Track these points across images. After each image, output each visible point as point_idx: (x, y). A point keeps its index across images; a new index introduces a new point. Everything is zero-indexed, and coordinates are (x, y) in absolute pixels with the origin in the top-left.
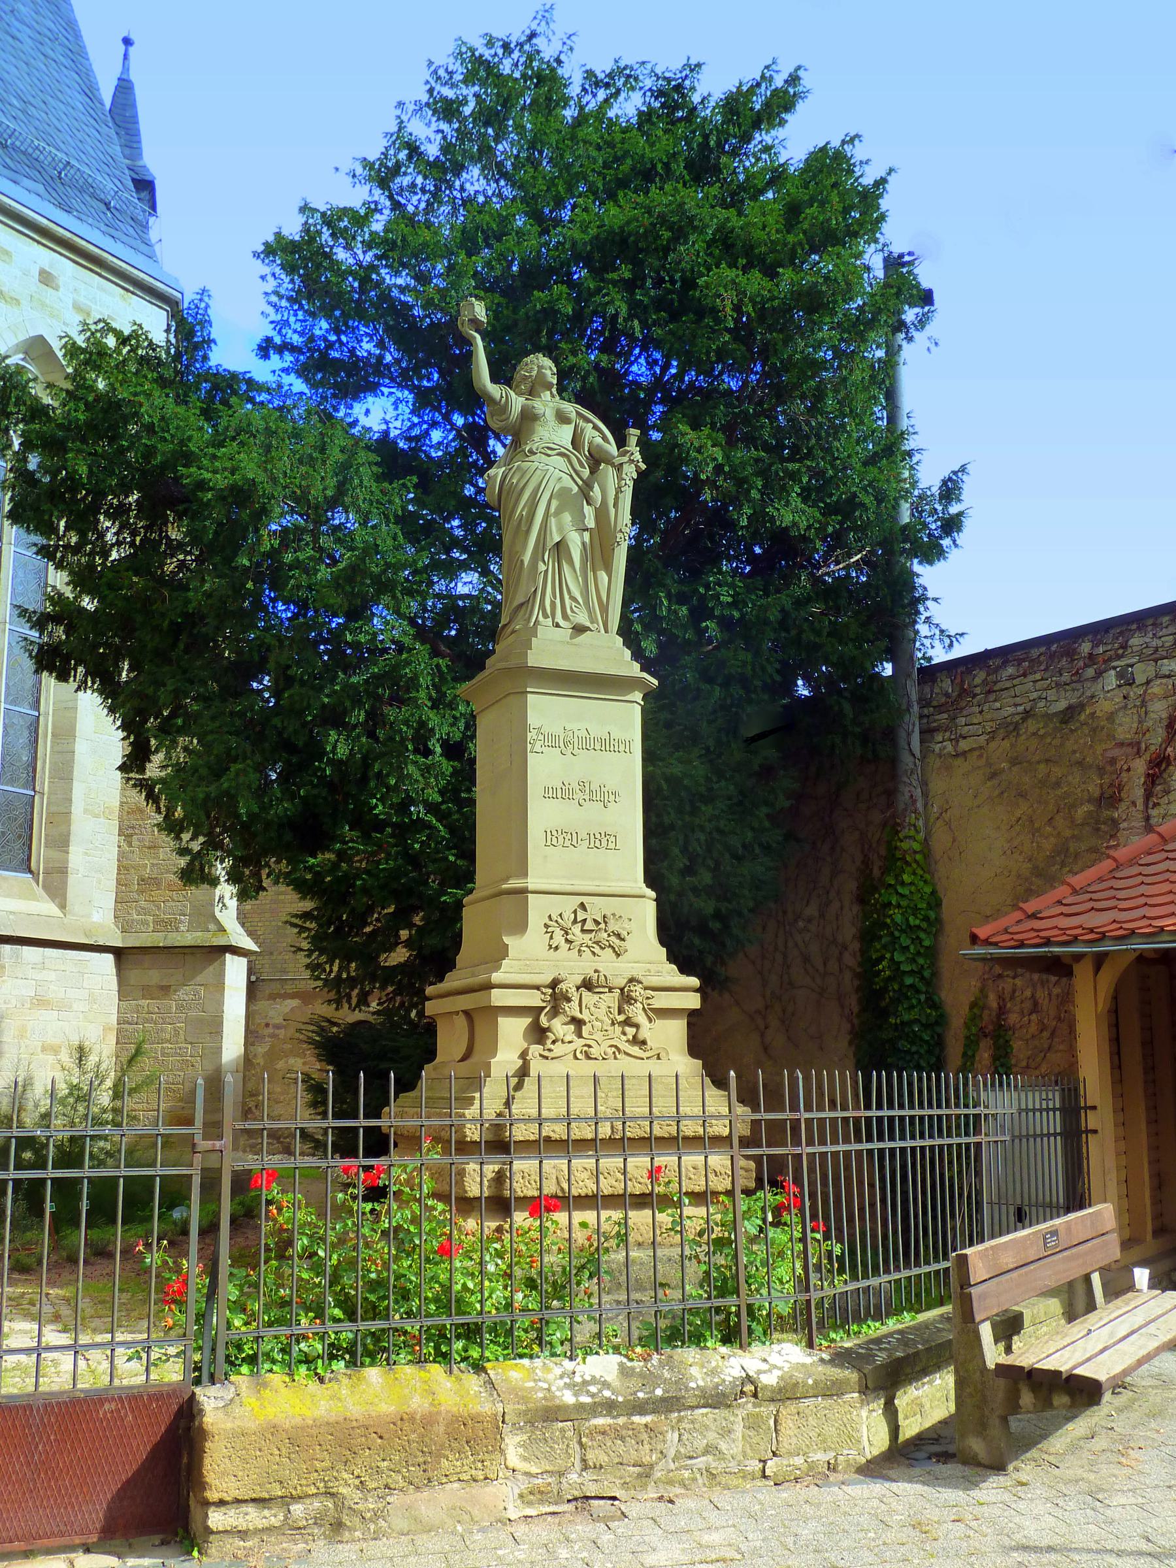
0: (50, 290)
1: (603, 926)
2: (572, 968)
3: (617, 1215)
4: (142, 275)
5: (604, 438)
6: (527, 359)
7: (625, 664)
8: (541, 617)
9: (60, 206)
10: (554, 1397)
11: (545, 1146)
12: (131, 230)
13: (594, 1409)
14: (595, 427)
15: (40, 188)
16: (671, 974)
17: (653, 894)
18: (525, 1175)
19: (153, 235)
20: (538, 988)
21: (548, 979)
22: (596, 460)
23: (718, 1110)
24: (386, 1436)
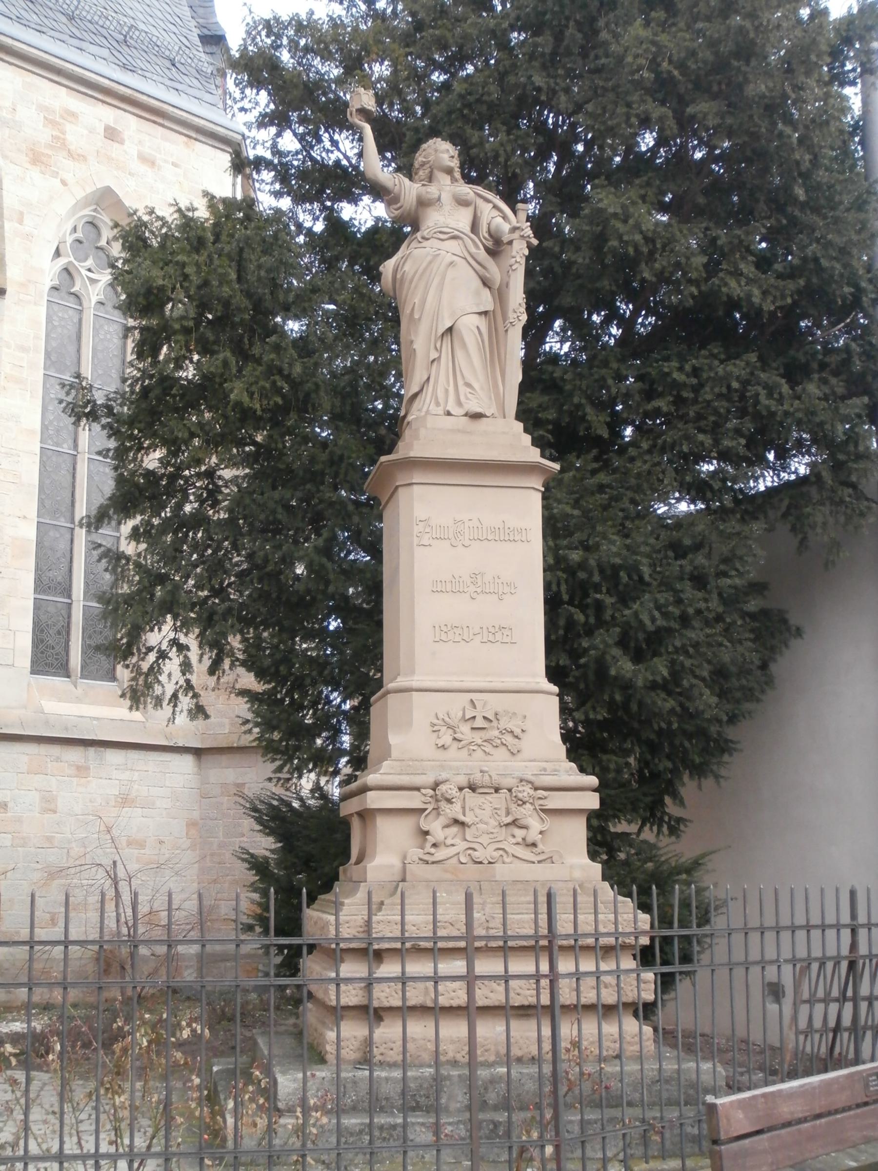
0: (116, 145)
1: (495, 724)
2: (458, 766)
3: (499, 1027)
4: (202, 122)
6: (424, 146)
7: (521, 447)
9: (124, 67)
12: (195, 82)
14: (495, 207)
15: (105, 53)
16: (569, 773)
17: (556, 689)
20: (418, 789)
21: (429, 779)
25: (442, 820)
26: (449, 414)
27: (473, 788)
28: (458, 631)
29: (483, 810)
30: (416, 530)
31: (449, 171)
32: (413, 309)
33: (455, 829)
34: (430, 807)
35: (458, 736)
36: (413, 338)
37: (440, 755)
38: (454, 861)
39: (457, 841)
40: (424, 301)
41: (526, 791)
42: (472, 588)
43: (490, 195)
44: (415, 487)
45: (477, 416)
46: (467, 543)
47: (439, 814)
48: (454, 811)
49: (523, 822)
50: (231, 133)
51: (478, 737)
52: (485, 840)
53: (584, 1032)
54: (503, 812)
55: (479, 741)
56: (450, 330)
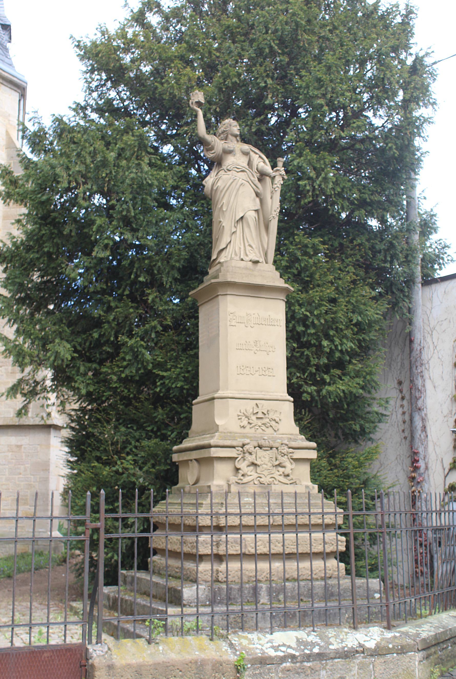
1: (267, 416)
4: (6, 75)
5: (264, 162)
8: (233, 256)
10: (264, 652)
11: (242, 528)
13: (283, 659)
14: (260, 157)
16: (302, 441)
17: (292, 399)
18: (231, 543)
19: (11, 53)
20: (234, 447)
22: (262, 176)
23: (331, 512)
24: (183, 670)
25: (246, 463)
26: (242, 260)
27: (260, 447)
28: (248, 369)
29: (264, 457)
30: (229, 317)
31: (236, 136)
32: (222, 206)
33: (252, 468)
34: (240, 457)
35: (250, 421)
36: (221, 220)
37: (243, 430)
38: (252, 483)
39: (253, 473)
40: (228, 202)
41: (285, 450)
42: (255, 348)
43: (257, 151)
44: (228, 296)
45: (256, 262)
46: (252, 325)
47: (244, 460)
48: (251, 459)
49: (283, 464)
50: (21, 82)
51: (259, 422)
52: (266, 473)
53: (313, 566)
54: (274, 459)
55: (260, 424)
56: (242, 218)
